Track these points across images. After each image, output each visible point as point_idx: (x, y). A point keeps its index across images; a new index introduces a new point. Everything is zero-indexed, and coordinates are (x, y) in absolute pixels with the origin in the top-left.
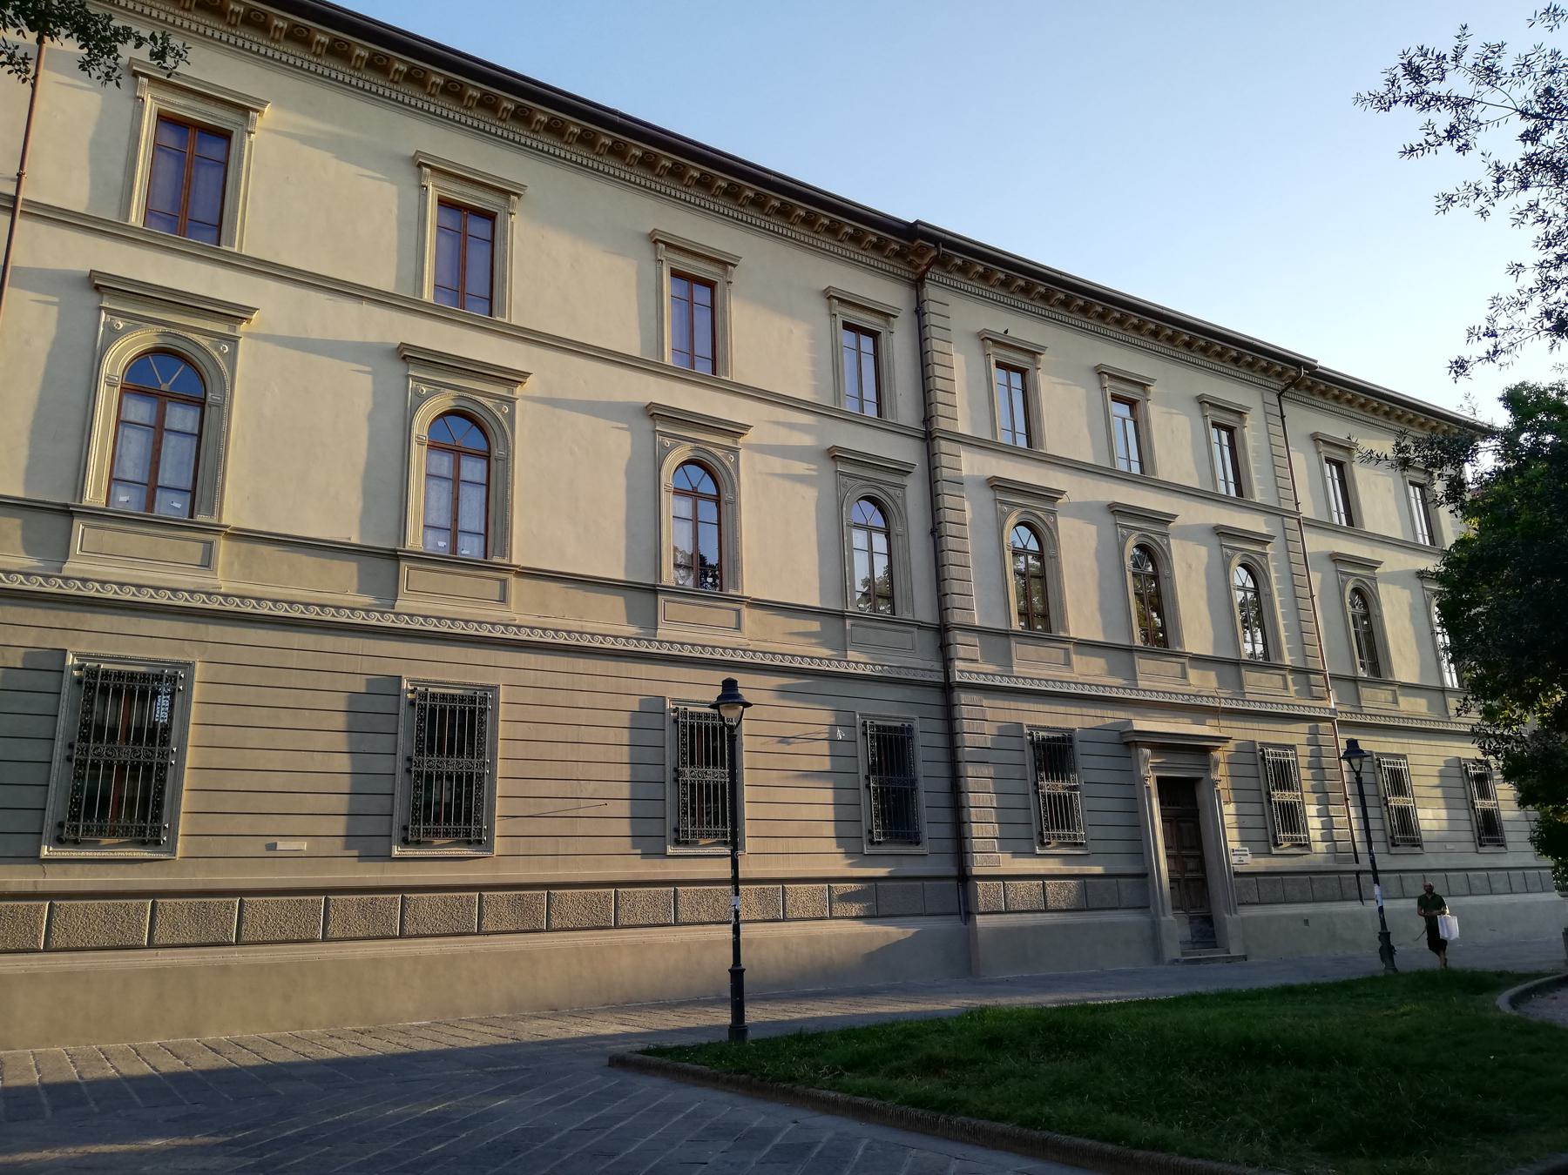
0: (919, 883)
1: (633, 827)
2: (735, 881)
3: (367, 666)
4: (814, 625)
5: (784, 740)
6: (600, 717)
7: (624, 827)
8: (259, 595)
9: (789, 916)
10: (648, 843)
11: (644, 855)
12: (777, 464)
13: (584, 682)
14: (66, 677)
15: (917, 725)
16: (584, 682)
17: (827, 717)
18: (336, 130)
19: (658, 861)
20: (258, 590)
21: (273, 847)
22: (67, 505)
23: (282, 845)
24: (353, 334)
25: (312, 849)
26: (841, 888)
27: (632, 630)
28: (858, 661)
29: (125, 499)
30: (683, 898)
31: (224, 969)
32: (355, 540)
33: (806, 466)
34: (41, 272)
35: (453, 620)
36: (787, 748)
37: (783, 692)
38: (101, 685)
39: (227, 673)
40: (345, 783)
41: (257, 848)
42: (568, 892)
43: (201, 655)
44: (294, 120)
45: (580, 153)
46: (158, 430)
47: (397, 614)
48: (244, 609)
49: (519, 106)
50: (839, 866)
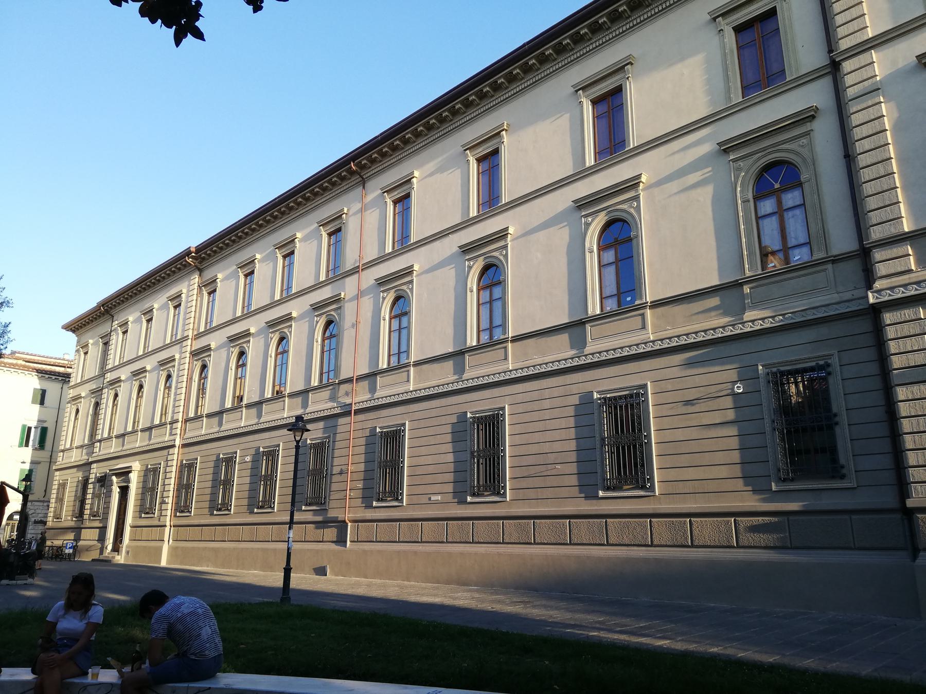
0: (846, 517)
1: (579, 480)
2: (291, 523)
3: (575, 389)
4: (714, 301)
5: (688, 403)
6: (556, 413)
7: (574, 480)
8: (889, 286)
9: (610, 542)
10: (588, 491)
11: (586, 498)
12: (674, 186)
13: (547, 393)
14: (595, 404)
15: (835, 361)
16: (547, 393)
17: (733, 375)
18: (445, 156)
19: (594, 502)
20: (547, 359)
21: (430, 499)
22: (737, 281)
23: (433, 498)
24: (437, 259)
25: (440, 500)
26: (745, 521)
27: (573, 352)
28: (756, 318)
29: (611, 305)
30: (450, 526)
31: (415, 553)
32: (451, 350)
33: (700, 173)
34: (689, 165)
35: (622, 348)
36: (690, 409)
37: (689, 364)
38: (612, 404)
39: (521, 408)
40: (451, 467)
41: (424, 499)
42: (543, 521)
43: (506, 402)
44: (431, 166)
45: (531, 78)
46: (780, 212)
47: (586, 356)
48: (908, 294)
49: (608, 15)
50: (751, 502)
